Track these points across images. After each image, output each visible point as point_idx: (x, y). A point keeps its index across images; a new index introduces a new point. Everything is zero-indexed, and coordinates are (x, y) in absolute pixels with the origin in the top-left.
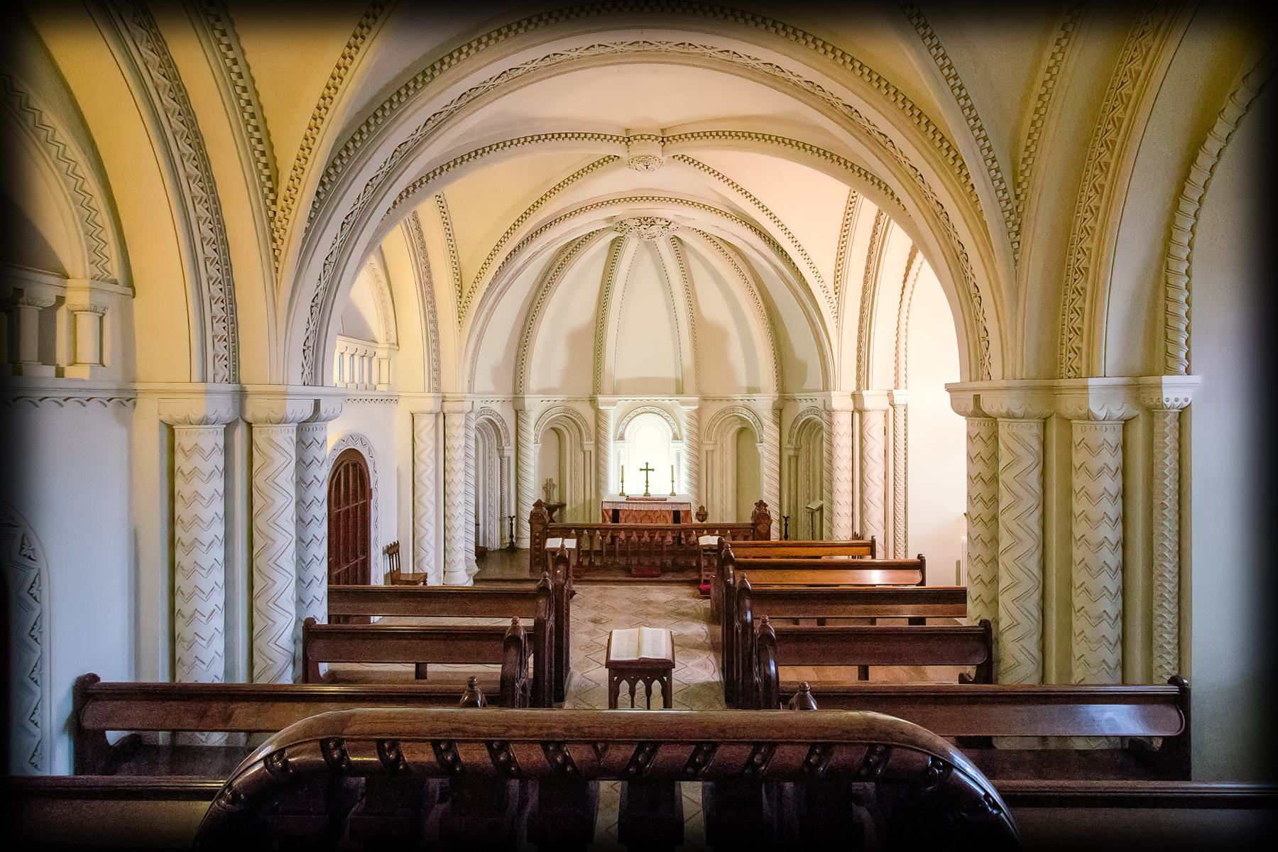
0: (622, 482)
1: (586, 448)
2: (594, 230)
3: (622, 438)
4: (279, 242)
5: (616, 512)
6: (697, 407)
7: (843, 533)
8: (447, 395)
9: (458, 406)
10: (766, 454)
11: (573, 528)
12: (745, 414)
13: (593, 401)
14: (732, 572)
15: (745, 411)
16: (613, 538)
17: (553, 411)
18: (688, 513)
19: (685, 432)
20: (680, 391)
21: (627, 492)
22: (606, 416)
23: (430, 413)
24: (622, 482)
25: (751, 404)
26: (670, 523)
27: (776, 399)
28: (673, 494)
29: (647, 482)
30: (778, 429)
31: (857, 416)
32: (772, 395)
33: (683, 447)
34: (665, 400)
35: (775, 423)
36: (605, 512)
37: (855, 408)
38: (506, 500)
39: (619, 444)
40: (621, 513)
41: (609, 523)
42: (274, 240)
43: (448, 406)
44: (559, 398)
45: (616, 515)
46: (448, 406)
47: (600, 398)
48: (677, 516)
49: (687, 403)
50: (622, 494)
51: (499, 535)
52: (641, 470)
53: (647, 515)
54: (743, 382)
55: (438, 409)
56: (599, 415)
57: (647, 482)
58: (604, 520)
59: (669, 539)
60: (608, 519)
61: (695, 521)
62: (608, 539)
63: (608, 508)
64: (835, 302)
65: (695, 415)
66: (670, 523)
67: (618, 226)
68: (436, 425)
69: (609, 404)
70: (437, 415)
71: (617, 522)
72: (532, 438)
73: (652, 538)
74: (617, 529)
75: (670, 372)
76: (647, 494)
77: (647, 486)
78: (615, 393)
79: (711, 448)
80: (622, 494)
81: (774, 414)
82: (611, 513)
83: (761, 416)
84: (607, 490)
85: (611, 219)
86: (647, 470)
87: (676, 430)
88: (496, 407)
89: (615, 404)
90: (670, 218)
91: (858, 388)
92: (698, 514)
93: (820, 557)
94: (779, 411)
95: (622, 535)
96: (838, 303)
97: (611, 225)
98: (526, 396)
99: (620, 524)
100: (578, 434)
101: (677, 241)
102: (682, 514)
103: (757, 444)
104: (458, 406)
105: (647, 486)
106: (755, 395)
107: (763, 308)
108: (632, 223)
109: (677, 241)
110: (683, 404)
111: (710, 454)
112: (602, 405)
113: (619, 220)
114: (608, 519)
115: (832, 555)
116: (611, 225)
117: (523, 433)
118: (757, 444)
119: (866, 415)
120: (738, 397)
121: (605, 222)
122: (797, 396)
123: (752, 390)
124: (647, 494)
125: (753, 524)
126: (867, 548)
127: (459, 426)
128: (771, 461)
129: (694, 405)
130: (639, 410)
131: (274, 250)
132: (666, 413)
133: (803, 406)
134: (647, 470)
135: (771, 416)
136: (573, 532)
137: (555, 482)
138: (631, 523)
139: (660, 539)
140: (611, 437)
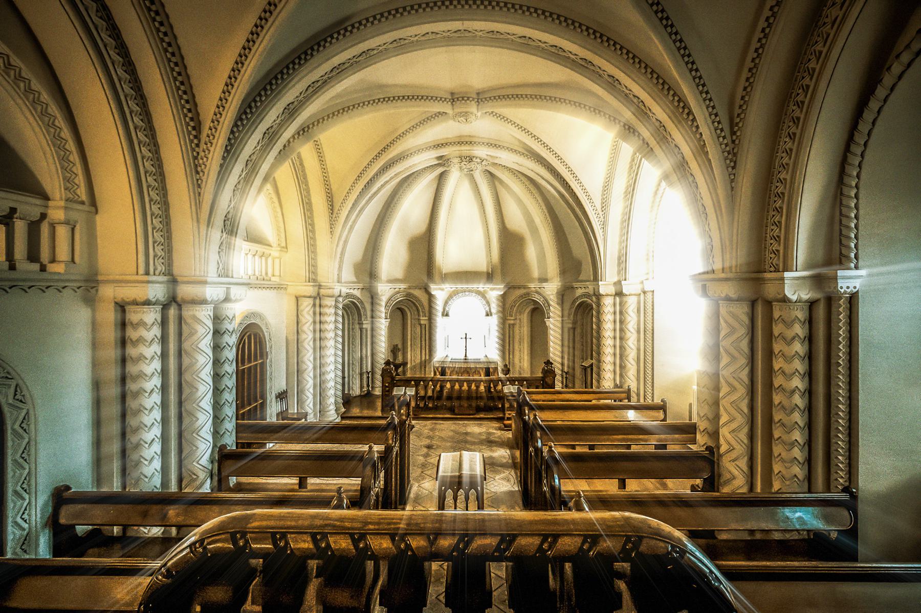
12: (537, 298)
21: (470, 356)
46: (322, 292)
61: (501, 375)
64: (602, 217)
79: (512, 322)
94: (564, 294)
95: (448, 385)
123: (543, 280)
137: (400, 346)
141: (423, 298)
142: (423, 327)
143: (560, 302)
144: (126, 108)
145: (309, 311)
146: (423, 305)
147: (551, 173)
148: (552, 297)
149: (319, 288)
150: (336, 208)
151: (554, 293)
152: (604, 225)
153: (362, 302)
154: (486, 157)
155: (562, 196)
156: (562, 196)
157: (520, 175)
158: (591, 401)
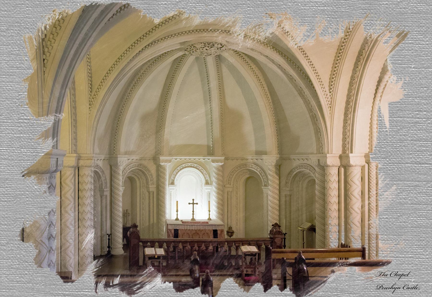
0: (177, 211)
1: (151, 190)
2: (169, 50)
3: (172, 183)
4: (48, 54)
5: (176, 231)
6: (223, 164)
7: (333, 244)
8: (82, 155)
9: (88, 162)
10: (270, 193)
11: (148, 242)
12: (254, 169)
13: (155, 159)
14: (305, 268)
15: (254, 166)
16: (175, 248)
17: (131, 165)
18: (222, 231)
19: (214, 179)
20: (210, 152)
21: (180, 218)
22: (165, 169)
23: (72, 167)
24: (177, 211)
25: (259, 162)
26: (172, 238)
27: (278, 158)
28: (209, 219)
29: (193, 212)
30: (278, 178)
31: (342, 170)
32: (275, 156)
33: (212, 190)
34: (201, 159)
35: (276, 173)
36: (168, 230)
37: (341, 165)
38: (105, 224)
39: (171, 187)
40: (179, 231)
41: (172, 238)
42: (44, 53)
43: (81, 163)
44: (135, 157)
45: (176, 233)
46: (81, 163)
47: (161, 158)
48: (215, 232)
49: (217, 161)
50: (177, 219)
51: (100, 246)
52: (189, 204)
53: (197, 232)
54: (253, 148)
55: (76, 165)
56: (160, 170)
57: (193, 212)
58: (169, 236)
59: (211, 248)
60: (171, 235)
61: (226, 237)
62: (171, 249)
63: (171, 228)
64: (330, 98)
65: (221, 168)
66: (211, 238)
67: (189, 47)
68: (75, 175)
69: (166, 161)
70: (75, 167)
71: (177, 237)
72: (121, 183)
73: (184, 247)
74: (177, 242)
75: (203, 141)
76: (193, 219)
77: (193, 214)
78: (170, 155)
79: (231, 190)
80: (177, 219)
81: (276, 168)
82: (173, 231)
83: (265, 168)
84: (164, 216)
85: (181, 44)
86: (193, 204)
87: (208, 178)
88: (100, 163)
89: (170, 161)
90: (224, 43)
91: (344, 151)
92: (228, 232)
93: (314, 259)
94: (279, 167)
95: (180, 246)
96: (331, 98)
97: (183, 46)
98: (118, 156)
99: (179, 238)
100: (145, 181)
101: (219, 59)
102: (219, 232)
103: (262, 187)
104: (88, 162)
105: (193, 214)
106: (263, 156)
107: (270, 101)
108: (198, 46)
109: (219, 59)
110: (213, 161)
111: (229, 194)
112: (162, 163)
113: (190, 44)
114: (171, 235)
115: (324, 258)
116: (183, 46)
117: (115, 180)
118: (262, 187)
119: (351, 169)
120: (250, 157)
121: (179, 45)
122: (292, 157)
123: (260, 153)
124: (193, 219)
125: (271, 238)
126: (360, 253)
127: (88, 175)
128: (274, 198)
129: (221, 163)
130: (184, 165)
131: (44, 60)
132: (201, 167)
133: (296, 163)
134: (193, 204)
135: (274, 170)
136: (157, 244)
137: (129, 212)
138: (186, 238)
139: (205, 248)
140: (167, 183)
141: (153, 168)
142: (152, 193)
143: (278, 172)
144: (372, 44)
145: (71, 180)
146: (151, 175)
147: (285, 59)
148: (270, 167)
149: (79, 159)
150: (95, 87)
151: (273, 164)
152: (331, 106)
153: (103, 172)
154: (226, 43)
155: (291, 78)
156: (291, 78)
157: (246, 58)
158: (314, 259)
